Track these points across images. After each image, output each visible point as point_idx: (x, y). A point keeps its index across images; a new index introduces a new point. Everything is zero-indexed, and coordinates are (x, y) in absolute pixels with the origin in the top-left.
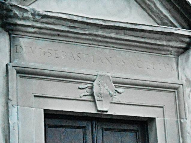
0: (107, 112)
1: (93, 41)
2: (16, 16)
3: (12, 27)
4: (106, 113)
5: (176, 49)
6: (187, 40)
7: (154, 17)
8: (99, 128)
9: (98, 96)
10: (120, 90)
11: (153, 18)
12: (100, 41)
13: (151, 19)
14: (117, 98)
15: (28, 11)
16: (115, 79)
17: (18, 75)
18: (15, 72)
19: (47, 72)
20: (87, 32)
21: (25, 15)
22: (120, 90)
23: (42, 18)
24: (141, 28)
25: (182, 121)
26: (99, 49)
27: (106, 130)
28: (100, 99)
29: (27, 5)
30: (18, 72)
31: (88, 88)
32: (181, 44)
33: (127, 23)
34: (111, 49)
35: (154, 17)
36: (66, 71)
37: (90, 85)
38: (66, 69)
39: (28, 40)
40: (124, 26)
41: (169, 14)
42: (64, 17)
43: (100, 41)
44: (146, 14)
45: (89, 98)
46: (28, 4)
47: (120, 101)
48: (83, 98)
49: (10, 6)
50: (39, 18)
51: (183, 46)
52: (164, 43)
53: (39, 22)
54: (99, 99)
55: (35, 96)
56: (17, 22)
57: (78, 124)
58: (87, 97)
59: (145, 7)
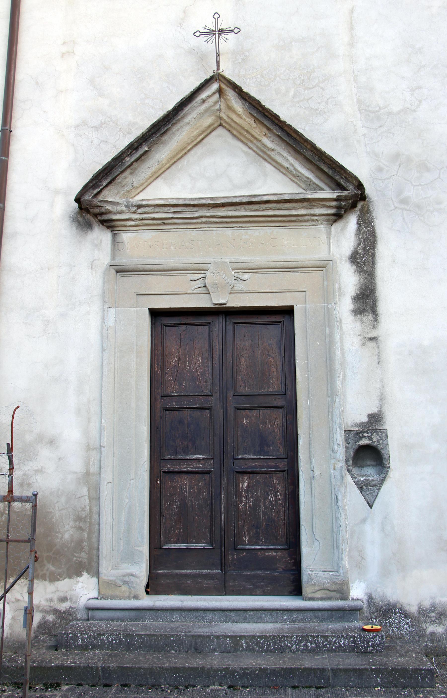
0: (226, 304)
1: (209, 224)
2: (110, 212)
3: (110, 224)
4: (225, 306)
5: (327, 218)
6: (334, 203)
7: (298, 182)
8: (228, 322)
9: (213, 287)
10: (245, 277)
11: (296, 183)
12: (218, 223)
13: (295, 185)
14: (240, 287)
15: (120, 204)
16: (236, 266)
17: (118, 274)
18: (114, 272)
19: (148, 267)
20: (196, 215)
21: (119, 208)
22: (245, 277)
23: (138, 209)
24: (262, 200)
25: (330, 306)
26: (218, 232)
27: (237, 324)
28: (216, 290)
29: (132, 196)
30: (117, 272)
31: (202, 279)
32: (327, 211)
33: (244, 196)
34: (235, 230)
35: (298, 182)
36: (173, 263)
37: (203, 275)
38: (173, 261)
39: (131, 234)
40: (239, 201)
41: (313, 175)
42: (161, 203)
43: (218, 223)
44: (287, 179)
45: (203, 290)
46: (133, 195)
47: (244, 289)
48: (194, 292)
49: (98, 203)
50: (135, 209)
51: (332, 211)
52: (303, 212)
53: (138, 213)
54: (213, 290)
55: (137, 295)
56: (112, 218)
57: (203, 320)
58: (200, 289)
59: (284, 172)
